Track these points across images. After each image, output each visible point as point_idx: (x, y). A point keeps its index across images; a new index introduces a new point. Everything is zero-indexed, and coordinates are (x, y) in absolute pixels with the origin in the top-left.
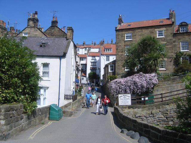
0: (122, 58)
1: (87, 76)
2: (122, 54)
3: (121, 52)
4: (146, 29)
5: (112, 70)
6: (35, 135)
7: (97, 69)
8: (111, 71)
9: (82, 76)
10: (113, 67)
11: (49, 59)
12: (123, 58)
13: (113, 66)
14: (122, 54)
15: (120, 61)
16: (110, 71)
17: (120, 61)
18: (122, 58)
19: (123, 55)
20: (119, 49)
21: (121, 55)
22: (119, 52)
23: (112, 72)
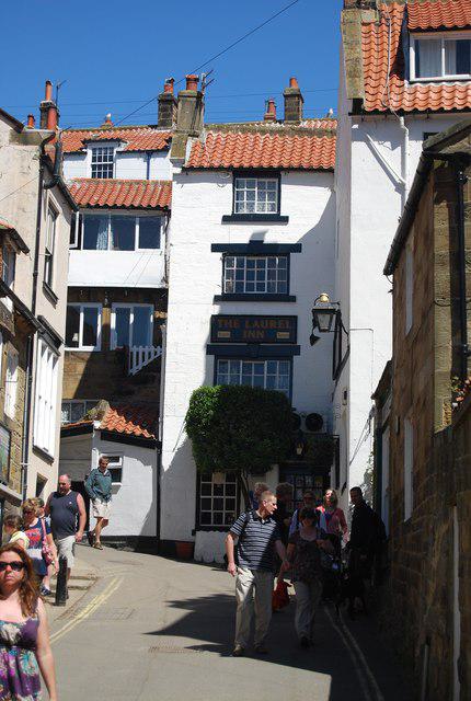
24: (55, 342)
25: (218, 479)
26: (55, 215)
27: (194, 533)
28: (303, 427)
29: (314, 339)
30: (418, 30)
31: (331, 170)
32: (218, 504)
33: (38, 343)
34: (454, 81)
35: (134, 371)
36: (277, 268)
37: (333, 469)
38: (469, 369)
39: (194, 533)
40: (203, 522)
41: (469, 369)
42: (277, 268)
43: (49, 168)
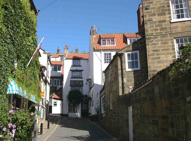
0: (162, 29)
1: (65, 97)
2: (162, 18)
3: (159, 15)
4: (61, 108)
5: (133, 67)
6: (47, 138)
7: (85, 82)
8: (130, 70)
9: (54, 99)
10: (136, 58)
11: (108, 66)
12: (166, 28)
13: (136, 54)
14: (162, 18)
15: (159, 38)
16: (128, 69)
17: (159, 38)
18: (162, 29)
19: (165, 21)
20: (154, 8)
21: (160, 22)
22: (154, 15)
23: (134, 71)
24: (49, 84)
25: (72, 105)
26: (49, 64)
27: (68, 113)
28: (84, 97)
29: (86, 84)
30: (103, 38)
31: (88, 59)
32: (108, 57)
33: (47, 84)
34: (123, 84)
35: (58, 89)
36: (179, 4)
37: (90, 101)
38: (105, 140)
39: (68, 113)
40: (70, 111)
41: (105, 140)
42: (179, 4)
43: (49, 58)
